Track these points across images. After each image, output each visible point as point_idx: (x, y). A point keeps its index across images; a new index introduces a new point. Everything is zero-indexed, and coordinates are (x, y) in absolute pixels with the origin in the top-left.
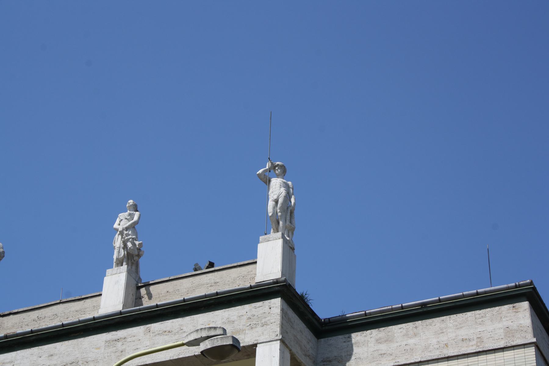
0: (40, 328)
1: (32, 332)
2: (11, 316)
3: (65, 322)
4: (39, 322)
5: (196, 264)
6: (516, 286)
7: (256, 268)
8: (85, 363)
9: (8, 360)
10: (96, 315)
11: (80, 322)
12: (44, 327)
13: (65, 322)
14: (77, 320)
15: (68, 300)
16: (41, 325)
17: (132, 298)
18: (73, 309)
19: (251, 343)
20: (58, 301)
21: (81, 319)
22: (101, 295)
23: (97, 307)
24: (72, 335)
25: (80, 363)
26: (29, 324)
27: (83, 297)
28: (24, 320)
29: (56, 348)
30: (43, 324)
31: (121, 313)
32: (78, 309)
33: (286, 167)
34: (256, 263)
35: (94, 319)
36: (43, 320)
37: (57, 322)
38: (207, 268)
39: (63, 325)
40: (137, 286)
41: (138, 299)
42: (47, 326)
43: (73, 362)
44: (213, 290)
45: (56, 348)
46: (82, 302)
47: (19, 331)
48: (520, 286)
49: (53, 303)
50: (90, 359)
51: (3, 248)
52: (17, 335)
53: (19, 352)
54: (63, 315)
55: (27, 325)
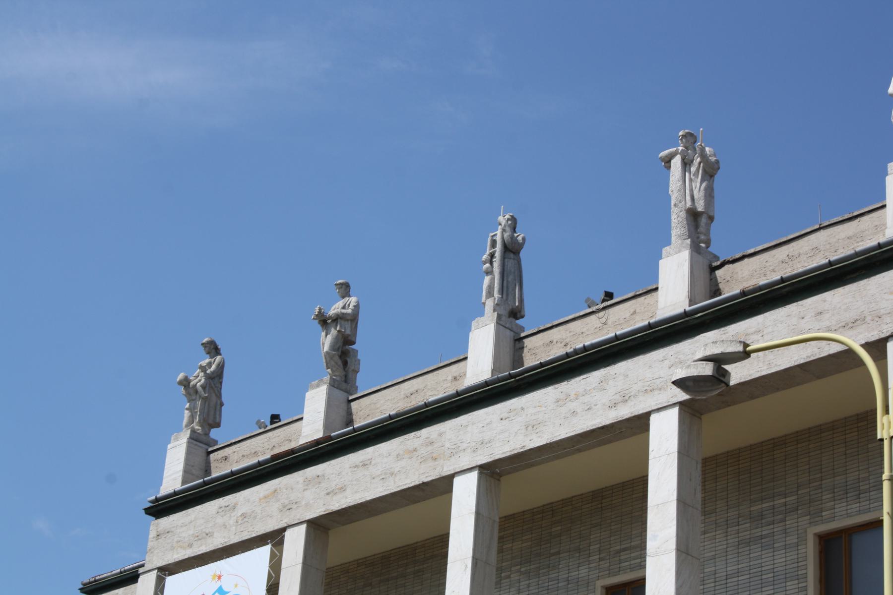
0: (795, 272)
1: (782, 280)
2: (746, 260)
3: (833, 258)
4: (791, 263)
5: (586, 301)
6: (121, 572)
7: (466, 366)
8: (877, 319)
9: (753, 330)
10: (882, 240)
11: (857, 254)
12: (801, 270)
13: (833, 259)
14: (852, 252)
15: (832, 221)
16: (795, 267)
17: (507, 359)
18: (842, 235)
19: (645, 411)
20: (817, 227)
21: (858, 249)
22: (884, 206)
23: (881, 227)
24: (848, 277)
25: (868, 319)
26: (776, 269)
27: (856, 213)
28: (768, 264)
29: (825, 301)
30: (799, 265)
31: (686, 314)
32: (850, 233)
33: (218, 343)
34: (657, 289)
35: (880, 246)
36: (798, 260)
37: (820, 260)
38: (272, 423)
39: (830, 263)
40: (707, 269)
41: (518, 360)
42: (804, 269)
43: (857, 320)
44: (254, 461)
45: (825, 301)
46: (855, 223)
47: (763, 282)
48: (125, 571)
49: (808, 230)
50: (883, 311)
51: (715, 155)
52: (760, 288)
53: (767, 314)
54: (828, 246)
55: (774, 271)
